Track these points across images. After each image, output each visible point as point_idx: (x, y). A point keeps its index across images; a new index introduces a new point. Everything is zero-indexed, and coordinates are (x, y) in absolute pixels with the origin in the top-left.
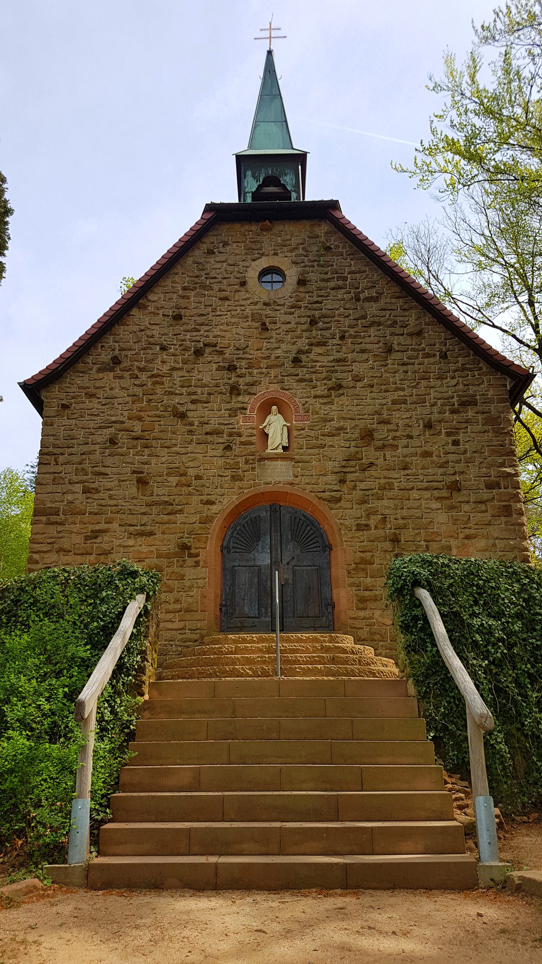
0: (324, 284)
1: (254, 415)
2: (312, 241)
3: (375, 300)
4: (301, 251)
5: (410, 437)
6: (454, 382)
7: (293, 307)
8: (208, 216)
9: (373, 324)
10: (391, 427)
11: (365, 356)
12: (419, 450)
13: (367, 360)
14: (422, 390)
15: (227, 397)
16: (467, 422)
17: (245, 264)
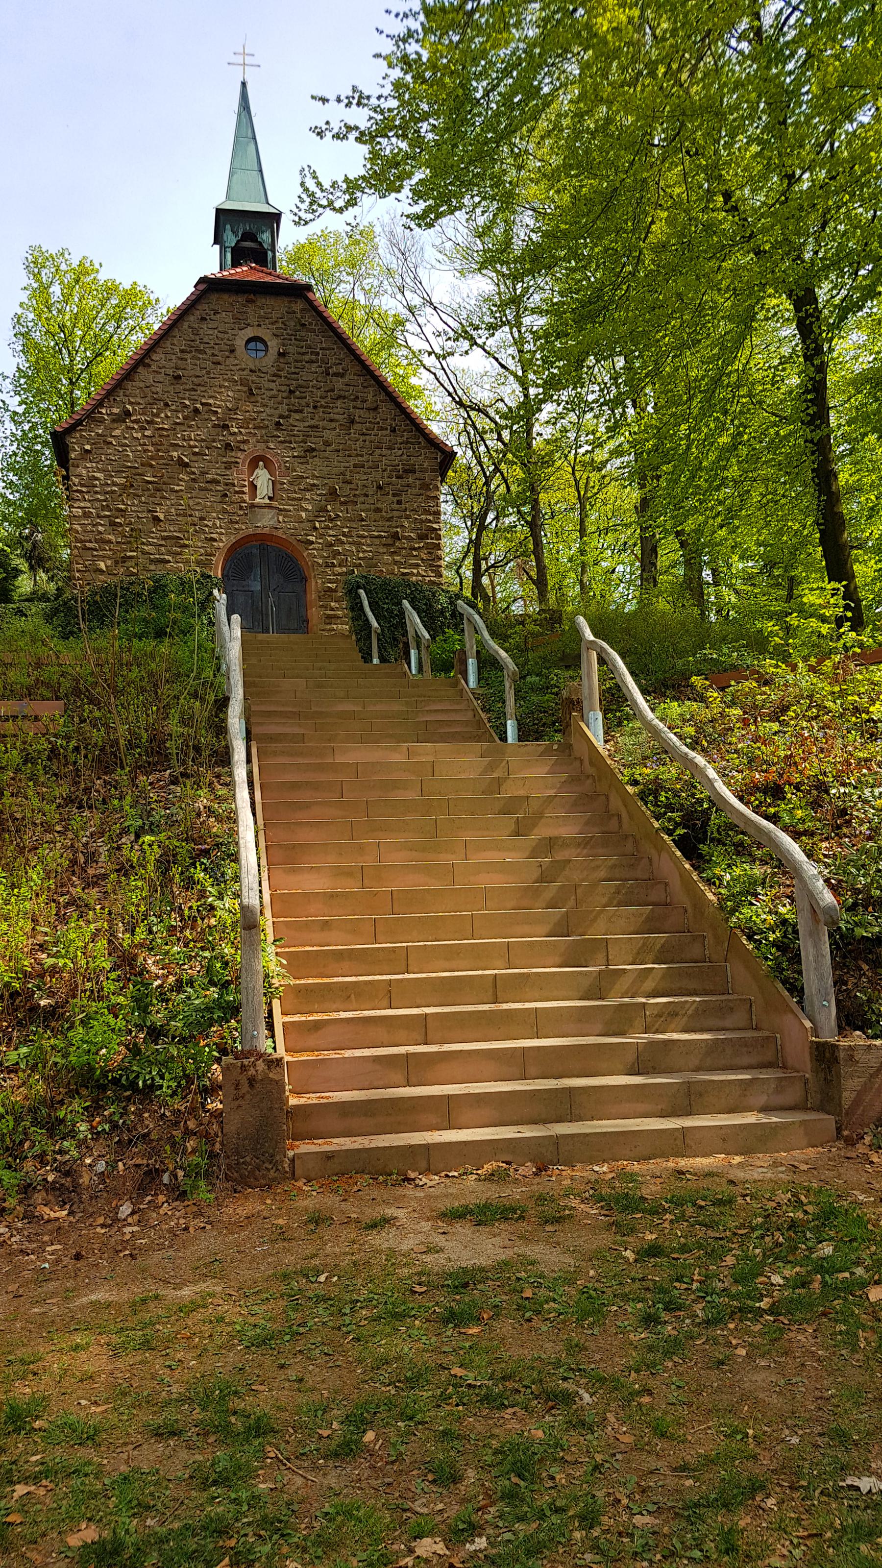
0: (300, 357)
1: (246, 468)
2: (290, 316)
3: (342, 375)
4: (280, 325)
5: (366, 495)
6: (400, 452)
7: (275, 375)
8: (202, 287)
9: (339, 397)
10: (352, 486)
11: (333, 425)
12: (373, 507)
13: (335, 429)
14: (376, 457)
15: (221, 452)
16: (408, 486)
17: (233, 332)
